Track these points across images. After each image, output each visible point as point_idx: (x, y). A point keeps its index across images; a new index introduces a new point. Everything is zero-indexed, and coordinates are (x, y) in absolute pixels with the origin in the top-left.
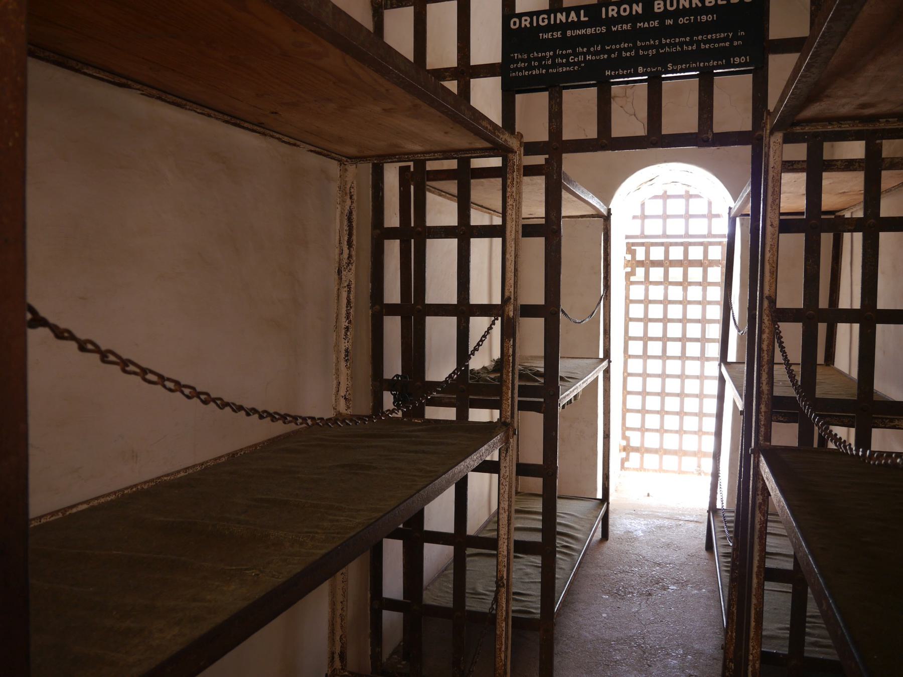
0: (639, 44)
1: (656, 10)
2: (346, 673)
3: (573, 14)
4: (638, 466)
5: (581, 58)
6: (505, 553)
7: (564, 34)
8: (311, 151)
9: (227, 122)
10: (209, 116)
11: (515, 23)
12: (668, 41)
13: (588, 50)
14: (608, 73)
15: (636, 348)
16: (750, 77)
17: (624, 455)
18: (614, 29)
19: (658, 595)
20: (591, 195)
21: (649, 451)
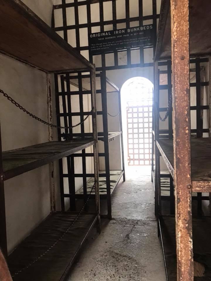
0: (124, 41)
1: (128, 32)
2: (56, 212)
3: (107, 33)
4: (133, 164)
5: (109, 45)
6: (97, 173)
7: (105, 39)
8: (39, 69)
9: (16, 59)
10: (12, 57)
11: (91, 36)
12: (132, 40)
13: (111, 42)
14: (117, 49)
15: (130, 136)
16: (153, 48)
17: (129, 161)
18: (118, 37)
19: (139, 192)
20: (114, 84)
21: (135, 160)
